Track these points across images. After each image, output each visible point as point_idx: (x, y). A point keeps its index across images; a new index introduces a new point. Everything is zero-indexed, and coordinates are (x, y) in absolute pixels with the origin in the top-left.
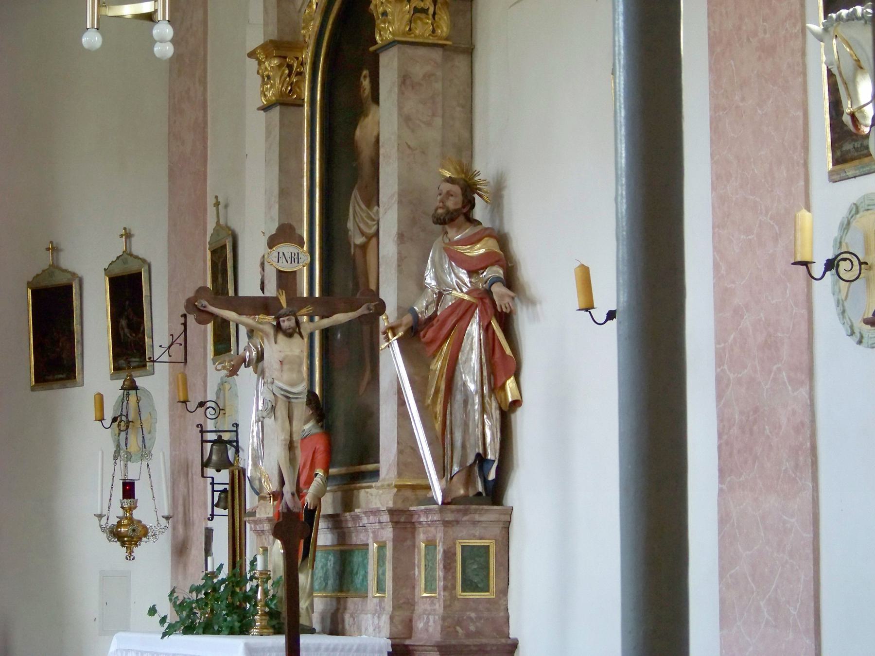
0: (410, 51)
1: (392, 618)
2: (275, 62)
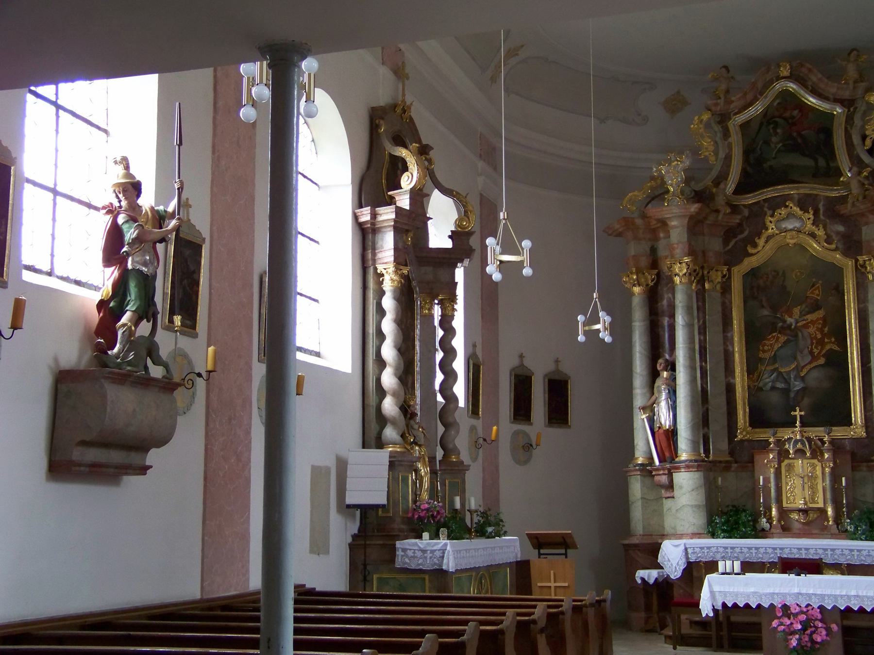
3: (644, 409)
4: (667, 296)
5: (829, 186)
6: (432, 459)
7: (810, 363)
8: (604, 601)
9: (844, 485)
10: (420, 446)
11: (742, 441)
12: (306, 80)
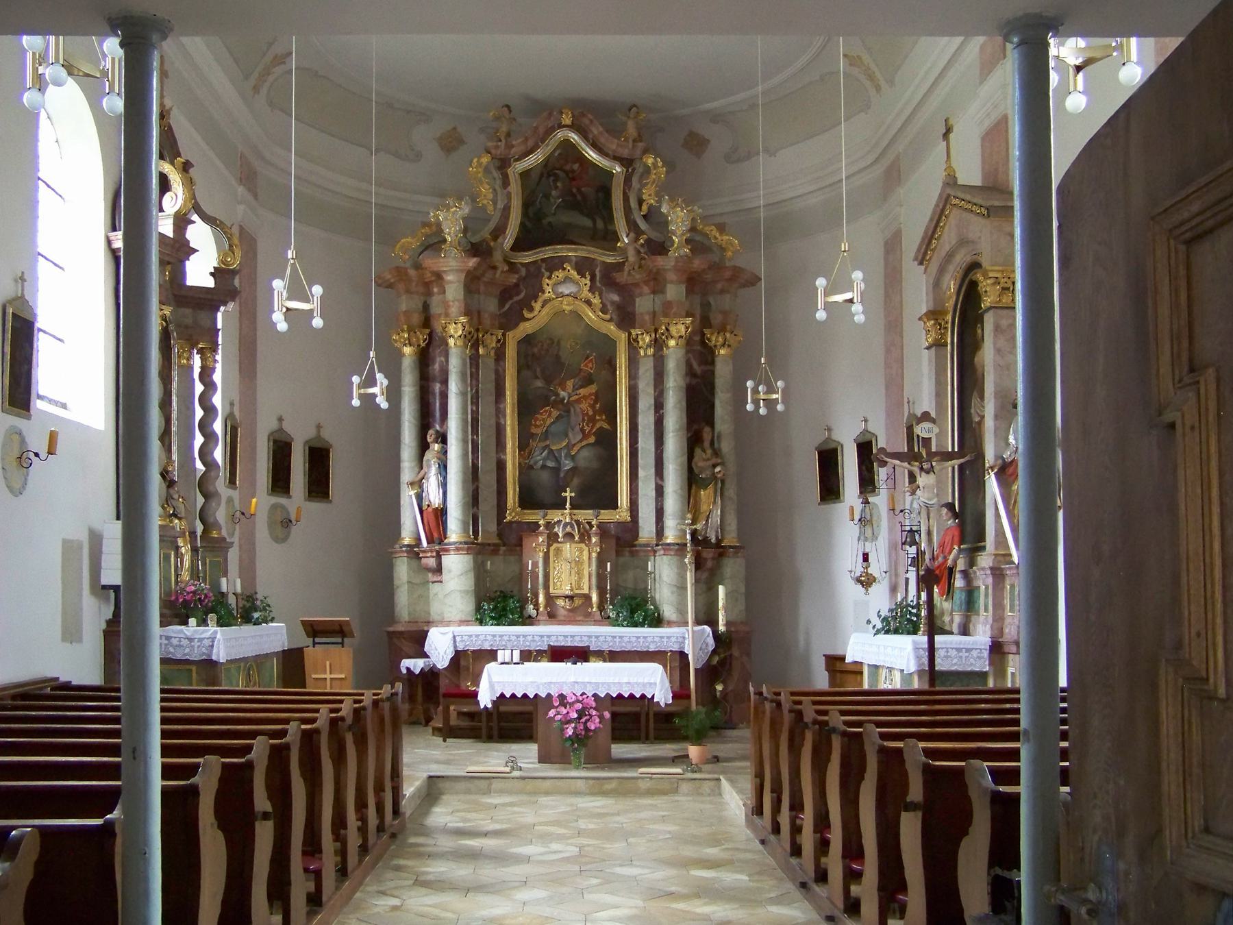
0: (999, 311)
1: (992, 627)
2: (932, 322)
3: (412, 484)
4: (439, 359)
5: (605, 250)
6: (193, 534)
7: (581, 441)
8: (396, 694)
9: (609, 570)
10: (180, 519)
11: (511, 523)
12: (109, 66)
